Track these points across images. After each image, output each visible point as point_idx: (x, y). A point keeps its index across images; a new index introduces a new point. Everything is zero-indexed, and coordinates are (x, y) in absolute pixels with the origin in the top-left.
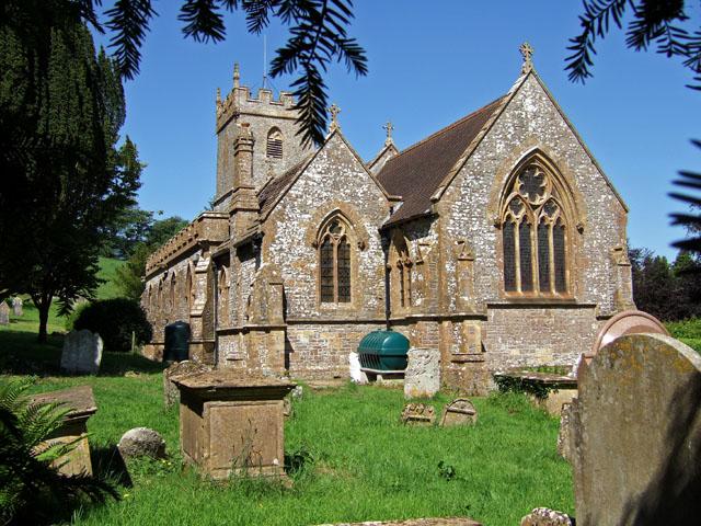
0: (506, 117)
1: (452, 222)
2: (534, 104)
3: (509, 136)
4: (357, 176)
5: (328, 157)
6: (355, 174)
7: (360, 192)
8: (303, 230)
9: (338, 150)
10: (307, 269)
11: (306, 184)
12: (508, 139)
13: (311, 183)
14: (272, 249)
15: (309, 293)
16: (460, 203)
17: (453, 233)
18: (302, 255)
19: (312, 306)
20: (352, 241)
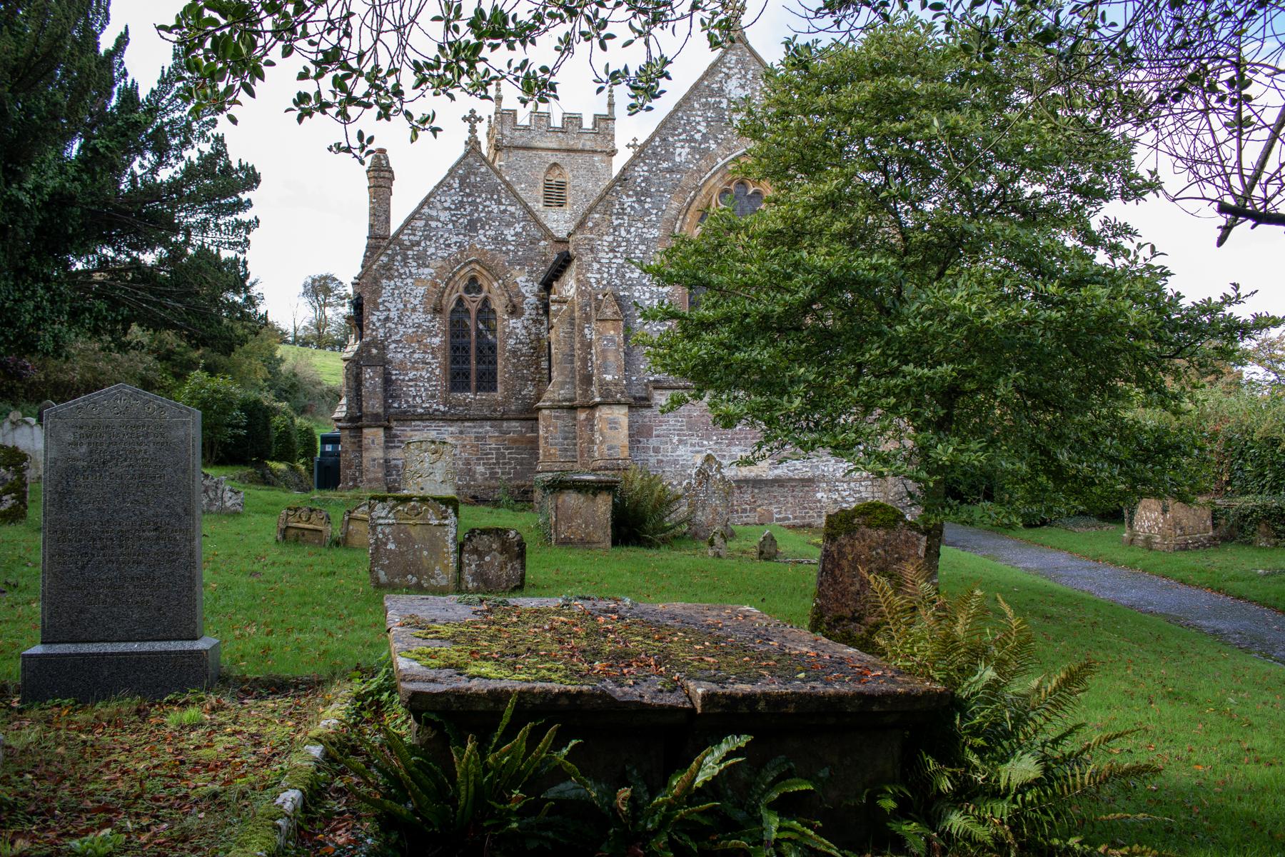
0: (693, 108)
1: (596, 266)
2: (742, 87)
3: (698, 136)
4: (505, 210)
5: (461, 184)
6: (502, 208)
7: (509, 234)
8: (421, 290)
9: (476, 175)
10: (425, 345)
11: (426, 225)
12: (695, 141)
13: (433, 224)
14: (374, 319)
15: (429, 380)
16: (611, 238)
17: (598, 282)
18: (420, 326)
19: (433, 397)
20: (498, 304)
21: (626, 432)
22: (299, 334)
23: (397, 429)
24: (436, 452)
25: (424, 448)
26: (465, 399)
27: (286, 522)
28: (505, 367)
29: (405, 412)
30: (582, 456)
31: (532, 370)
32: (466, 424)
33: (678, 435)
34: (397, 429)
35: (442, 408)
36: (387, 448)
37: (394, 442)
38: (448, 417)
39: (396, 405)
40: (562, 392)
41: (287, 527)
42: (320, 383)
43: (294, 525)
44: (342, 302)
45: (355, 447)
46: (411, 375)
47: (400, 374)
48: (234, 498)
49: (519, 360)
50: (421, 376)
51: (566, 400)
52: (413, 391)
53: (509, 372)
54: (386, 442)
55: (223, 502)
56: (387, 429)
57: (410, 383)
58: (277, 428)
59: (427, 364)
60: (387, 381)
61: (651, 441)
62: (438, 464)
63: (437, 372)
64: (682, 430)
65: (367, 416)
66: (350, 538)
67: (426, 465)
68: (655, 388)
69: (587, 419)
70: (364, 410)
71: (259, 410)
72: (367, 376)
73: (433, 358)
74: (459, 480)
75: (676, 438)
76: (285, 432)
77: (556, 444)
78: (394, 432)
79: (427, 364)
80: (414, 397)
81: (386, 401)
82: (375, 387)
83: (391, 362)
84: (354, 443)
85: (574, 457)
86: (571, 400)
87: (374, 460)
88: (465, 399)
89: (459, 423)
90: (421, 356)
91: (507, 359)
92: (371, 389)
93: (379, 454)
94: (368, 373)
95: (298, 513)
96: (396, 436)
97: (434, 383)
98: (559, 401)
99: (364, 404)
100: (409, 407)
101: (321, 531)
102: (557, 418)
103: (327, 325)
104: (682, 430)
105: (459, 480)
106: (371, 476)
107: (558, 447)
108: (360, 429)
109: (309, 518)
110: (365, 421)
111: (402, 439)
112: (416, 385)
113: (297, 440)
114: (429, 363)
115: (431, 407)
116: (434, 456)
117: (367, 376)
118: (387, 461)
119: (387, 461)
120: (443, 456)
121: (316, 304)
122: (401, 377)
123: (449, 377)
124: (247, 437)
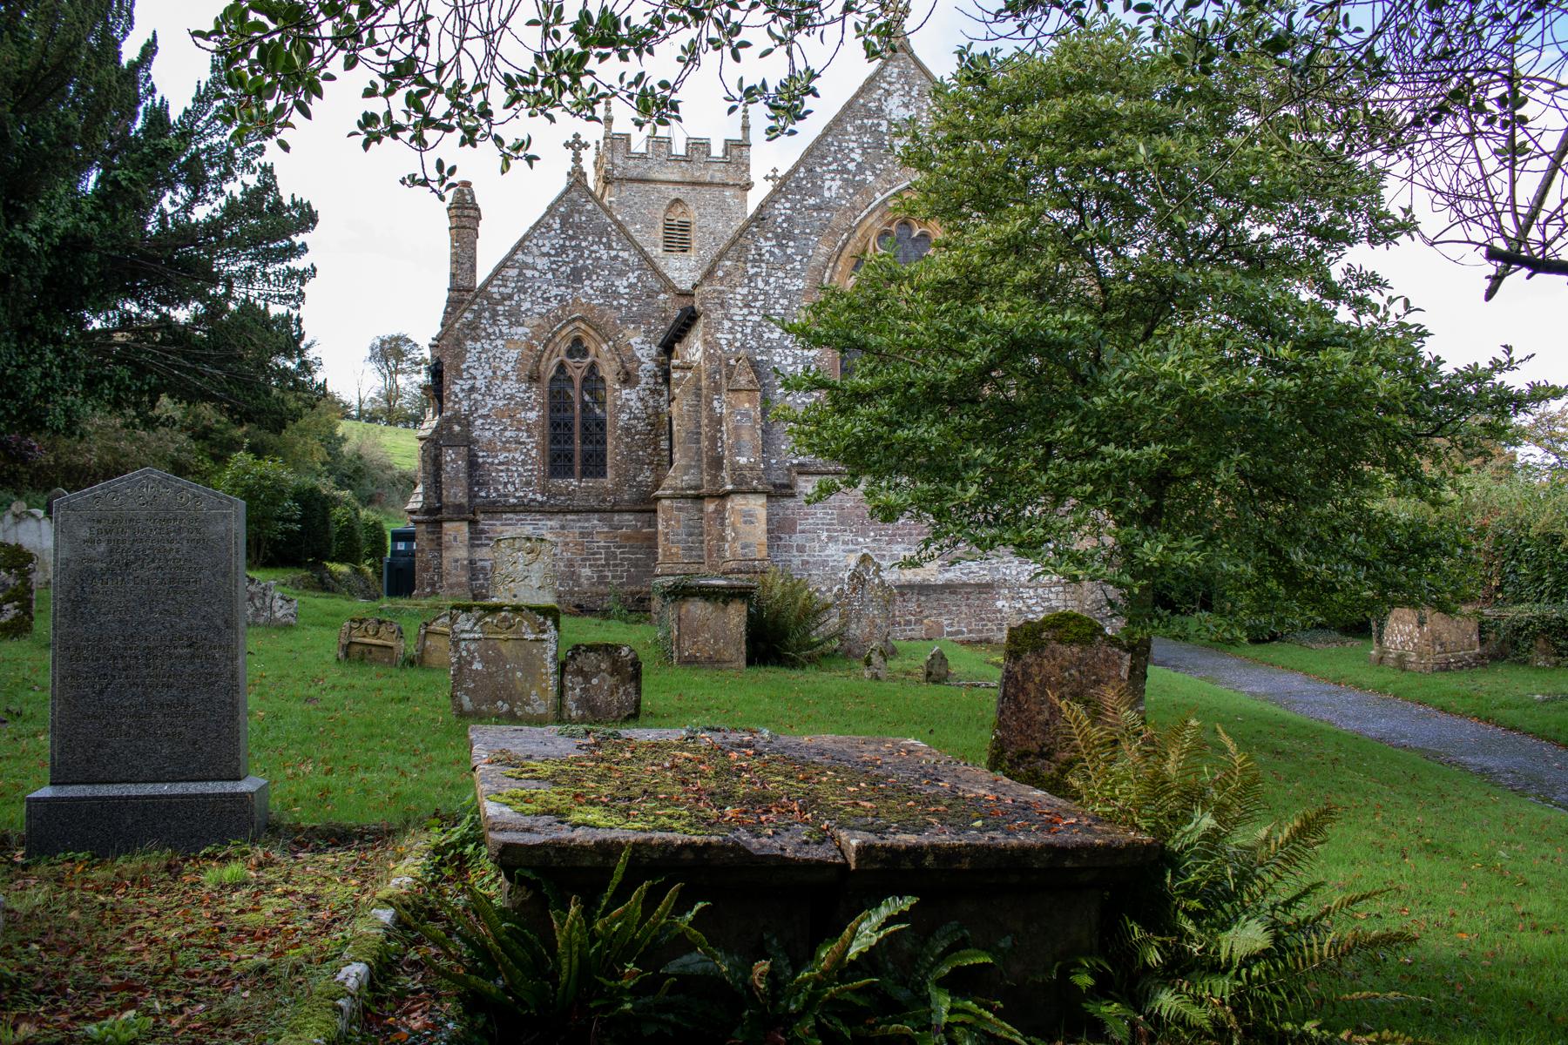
0: (846, 132)
1: (727, 324)
3: (852, 166)
4: (617, 257)
5: (562, 225)
6: (613, 253)
7: (621, 285)
8: (513, 354)
9: (580, 213)
10: (519, 421)
12: (849, 172)
13: (529, 273)
14: (457, 388)
15: (524, 463)
17: (730, 344)
18: (512, 397)
19: (528, 484)
20: (608, 370)
21: (764, 527)
22: (364, 407)
23: (485, 523)
24: (532, 551)
25: (517, 546)
26: (567, 487)
27: (350, 636)
28: (616, 447)
29: (494, 503)
30: (710, 556)
31: (649, 451)
32: (569, 517)
33: (827, 530)
34: (485, 523)
35: (539, 498)
36: (472, 546)
37: (480, 539)
38: (547, 508)
39: (483, 494)
40: (686, 478)
41: (351, 643)
42: (391, 467)
43: (359, 640)
44: (417, 368)
45: (433, 545)
46: (501, 458)
47: (488, 456)
48: (286, 607)
49: (633, 439)
50: (513, 458)
51: (690, 488)
52: (504, 477)
53: (621, 453)
54: (471, 538)
55: (273, 612)
56: (473, 523)
57: (501, 468)
58: (338, 522)
59: (521, 443)
60: (473, 464)
61: (794, 537)
62: (535, 566)
63: (533, 453)
64: (832, 524)
65: (447, 507)
66: (427, 656)
67: (520, 567)
68: (799, 473)
69: (716, 511)
70: (444, 500)
72: (448, 459)
73: (529, 437)
74: (561, 585)
75: (825, 534)
76: (347, 526)
77: (679, 542)
78: (481, 526)
79: (521, 443)
80: (506, 484)
81: (471, 489)
82: (458, 472)
83: (478, 441)
84: (432, 540)
85: (700, 557)
86: (696, 488)
87: (457, 561)
88: (567, 487)
89: (560, 516)
90: (513, 434)
91: (619, 438)
92: (452, 474)
93: (462, 553)
94: (449, 455)
95: (364, 626)
96: (483, 532)
97: (530, 467)
98: (682, 489)
99: (445, 493)
100: (499, 496)
101: (391, 648)
102: (680, 509)
103: (398, 396)
104: (832, 524)
105: (561, 585)
106: (453, 580)
107: (681, 545)
108: (439, 523)
109: (378, 632)
110: (445, 514)
111: (491, 535)
112: (508, 470)
113: (363, 536)
114: (524, 443)
115: (525, 496)
116: (530, 556)
117: (448, 459)
118: (472, 562)
119: (472, 562)
120: (541, 556)
121: (385, 371)
122: (490, 460)
123: (547, 460)
124: (301, 532)
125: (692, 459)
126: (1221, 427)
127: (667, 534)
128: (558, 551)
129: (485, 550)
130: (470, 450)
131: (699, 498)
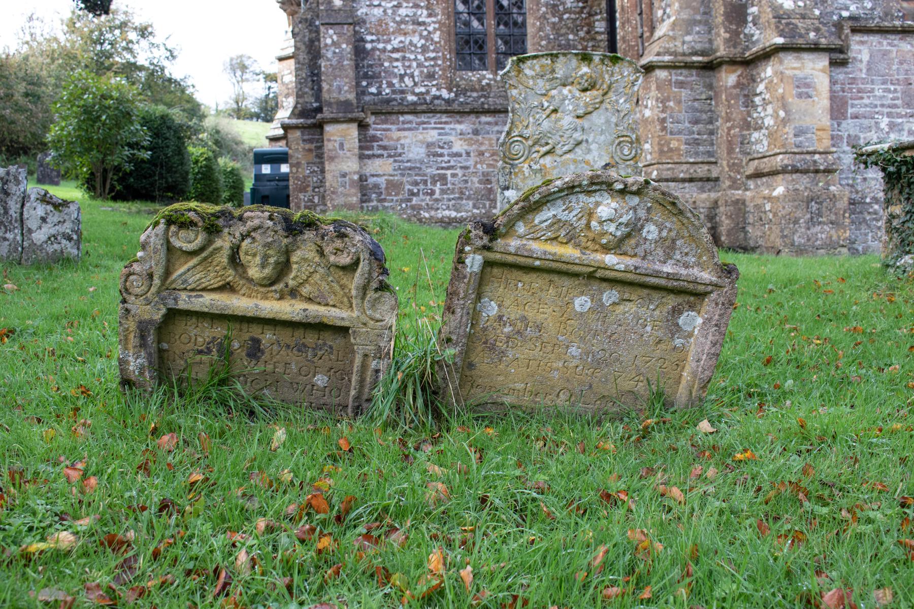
15: (425, 49)
19: (431, 76)
21: (826, 103)
22: (219, 108)
23: (377, 128)
24: (592, 86)
25: (560, 74)
26: (480, 81)
27: (167, 287)
28: (540, 29)
29: (388, 101)
30: (730, 151)
31: (582, 34)
32: (484, 119)
33: (889, 115)
34: (377, 128)
35: (445, 94)
36: (362, 157)
37: (371, 148)
38: (456, 106)
39: (373, 90)
40: (688, 38)
41: (173, 315)
42: (242, 143)
43: (207, 301)
44: (258, 77)
45: (312, 157)
46: (395, 43)
47: (378, 41)
48: (54, 218)
49: (561, 19)
50: (411, 43)
51: (695, 54)
52: (399, 66)
53: (547, 37)
54: (361, 148)
55: (25, 232)
56: (363, 126)
57: (395, 55)
58: (197, 162)
59: (420, 24)
60: (360, 52)
61: (844, 124)
62: (598, 119)
63: (436, 37)
64: (895, 106)
65: (330, 104)
66: (482, 362)
67: (567, 120)
68: (854, 31)
69: (738, 85)
70: (325, 96)
71: (169, 128)
72: (329, 41)
73: (430, 15)
74: (475, 206)
75: (886, 120)
76: (206, 166)
77: (680, 132)
78: (371, 132)
79: (420, 24)
80: (402, 77)
81: (358, 84)
82: (341, 58)
83: (364, 22)
84: (310, 150)
85: (710, 154)
86: (703, 53)
87: (344, 175)
88: (480, 81)
89: (472, 118)
90: (410, 12)
91: (544, 17)
92: (334, 62)
93: (351, 165)
94: (329, 37)
95: (224, 243)
96: (374, 139)
97: (432, 55)
98: (684, 54)
99: (325, 86)
100: (394, 92)
101: (343, 331)
102: (681, 85)
103: (244, 99)
104: (895, 106)
105: (475, 206)
106: (340, 201)
107: (683, 137)
108: (319, 127)
109: (284, 267)
110: (327, 114)
111: (385, 143)
112: (404, 58)
113: (222, 178)
114: (424, 23)
115: (428, 92)
116: (588, 97)
117: (329, 41)
118: (362, 179)
119: (362, 179)
120: (612, 96)
121: (234, 80)
122: (381, 46)
123: (454, 46)
124: (152, 162)
125: (696, 10)
126: (489, 199)
127: (663, 120)
128: (471, 162)
129: (378, 162)
130: (356, 32)
131: (711, 67)
